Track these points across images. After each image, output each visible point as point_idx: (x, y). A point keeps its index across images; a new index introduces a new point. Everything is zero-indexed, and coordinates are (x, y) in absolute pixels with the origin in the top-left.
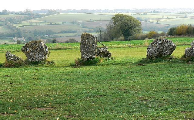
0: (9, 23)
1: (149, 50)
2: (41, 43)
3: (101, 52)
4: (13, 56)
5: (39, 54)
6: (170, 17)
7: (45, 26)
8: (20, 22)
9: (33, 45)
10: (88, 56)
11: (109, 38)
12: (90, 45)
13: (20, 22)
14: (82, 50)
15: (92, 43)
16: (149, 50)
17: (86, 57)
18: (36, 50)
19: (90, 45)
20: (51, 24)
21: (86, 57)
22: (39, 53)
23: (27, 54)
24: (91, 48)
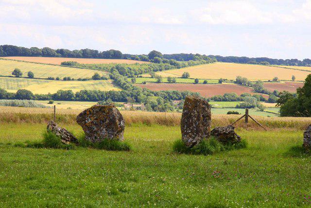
0: (116, 73)
1: (307, 136)
2: (112, 110)
3: (220, 134)
4: (59, 129)
5: (106, 130)
6: (35, 88)
7: (8, 78)
8: (139, 76)
9: (97, 112)
10: (194, 138)
11: (238, 61)
12: (198, 119)
13: (139, 76)
14: (184, 127)
15: (203, 116)
16: (307, 136)
17: (189, 141)
18: (103, 122)
19: (198, 119)
20: (196, 81)
21: (189, 141)
22: (108, 127)
23: (85, 127)
24: (201, 125)
